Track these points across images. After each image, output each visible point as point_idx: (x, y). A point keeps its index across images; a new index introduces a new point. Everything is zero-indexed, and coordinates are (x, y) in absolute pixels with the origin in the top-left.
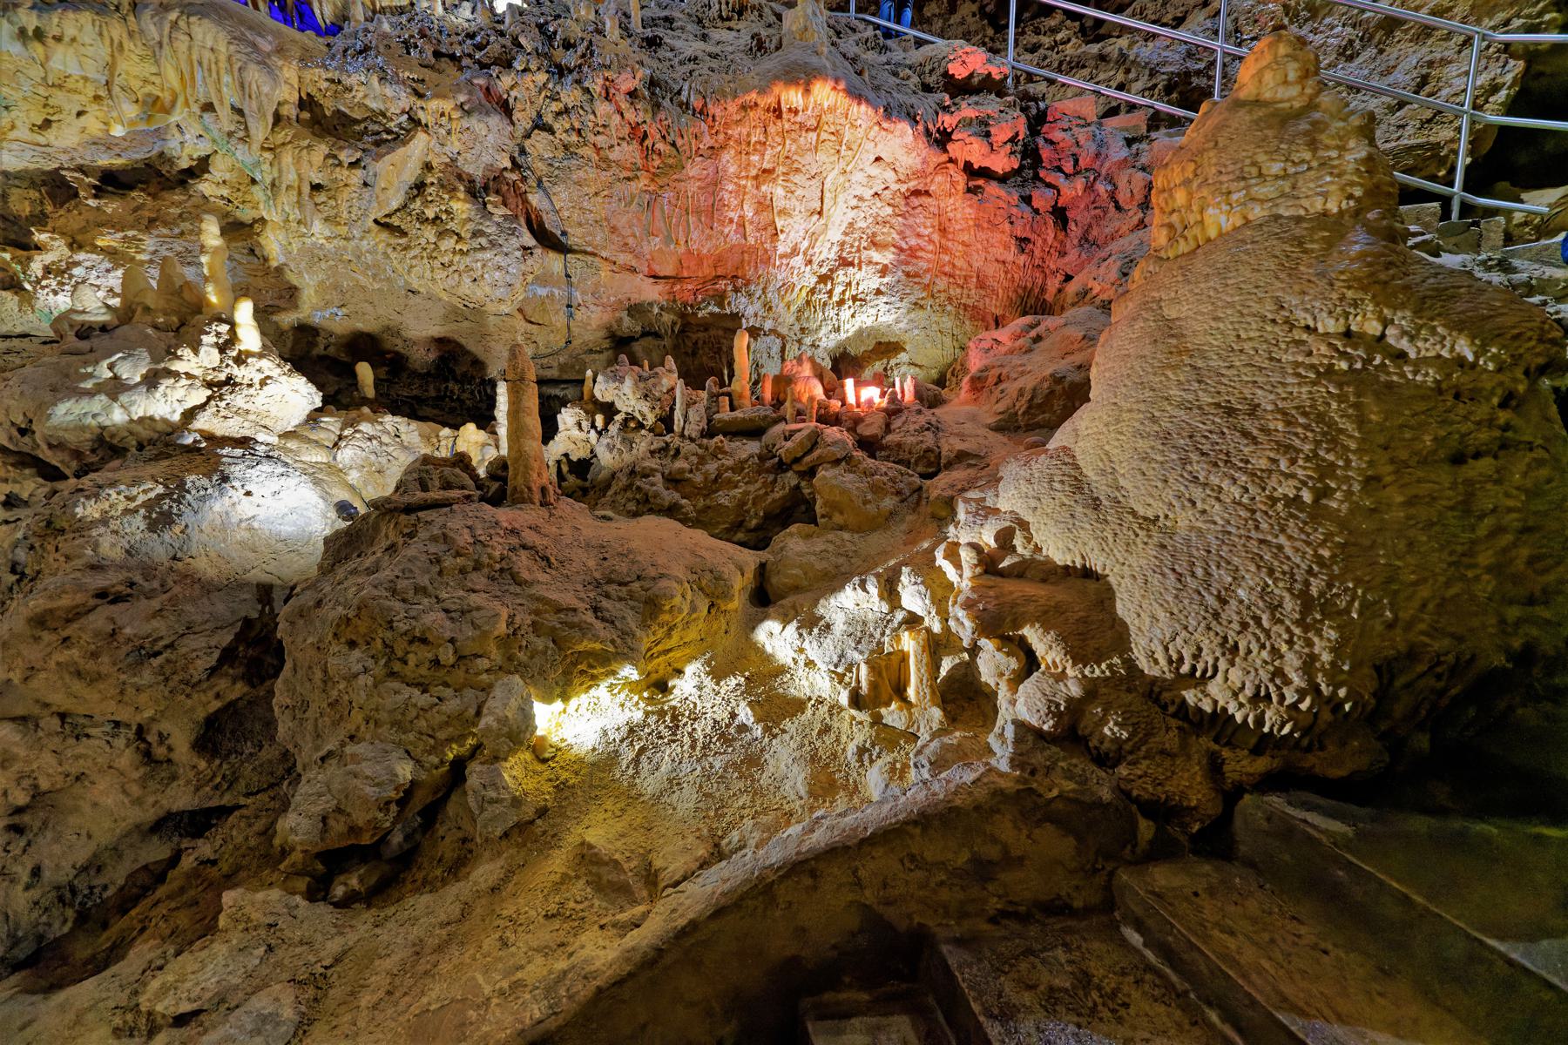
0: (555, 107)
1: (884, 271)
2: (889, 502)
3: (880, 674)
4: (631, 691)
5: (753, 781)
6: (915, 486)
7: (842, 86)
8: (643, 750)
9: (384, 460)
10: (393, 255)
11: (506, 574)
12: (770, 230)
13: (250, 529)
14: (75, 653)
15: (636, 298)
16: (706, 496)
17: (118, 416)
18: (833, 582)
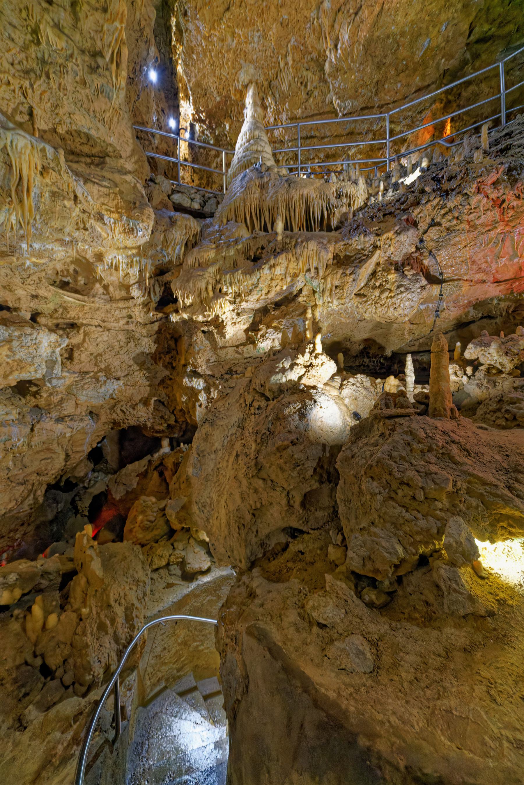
11: (446, 457)
17: (284, 380)
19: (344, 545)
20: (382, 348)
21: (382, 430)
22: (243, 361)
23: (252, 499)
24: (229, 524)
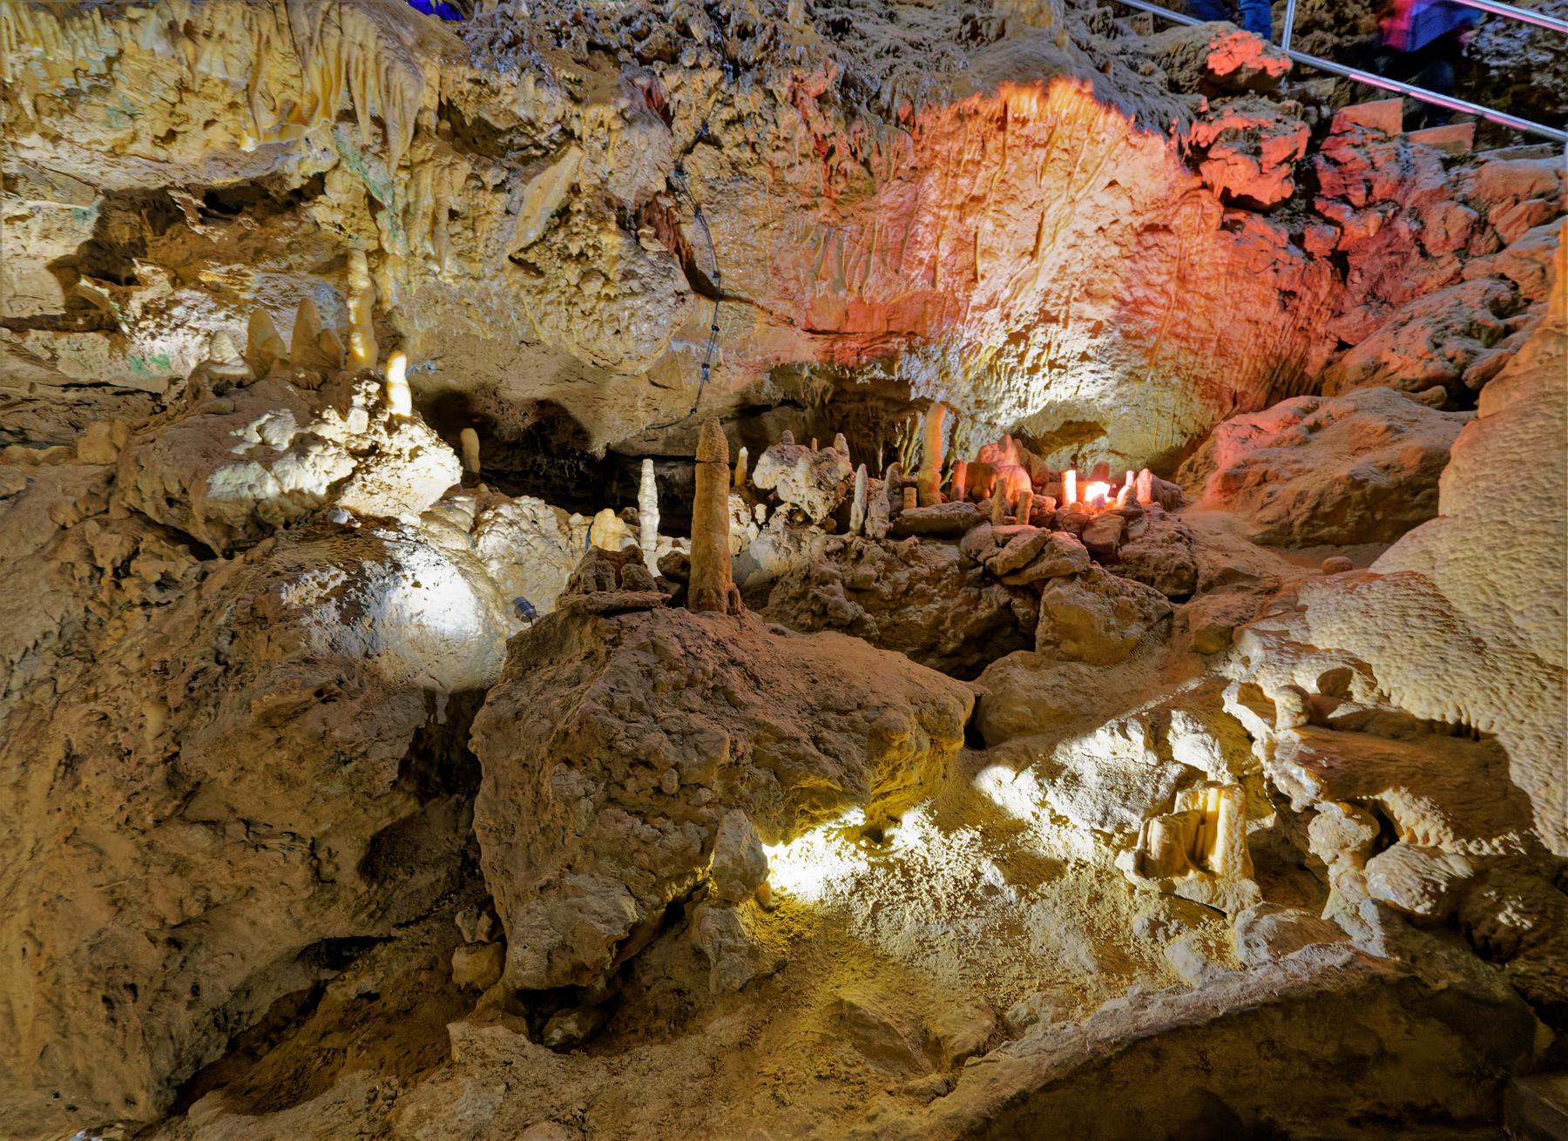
0: (727, 114)
1: (1096, 331)
2: (1135, 630)
3: (1176, 838)
4: (847, 838)
5: (1021, 949)
6: (1165, 611)
7: (1088, 89)
8: (877, 906)
9: (523, 550)
10: (527, 299)
11: (720, 694)
12: (968, 275)
13: (420, 625)
14: (284, 755)
15: (786, 358)
16: (892, 611)
17: (270, 489)
18: (1080, 723)
19: (498, 938)
20: (582, 435)
21: (589, 643)
22: (56, 393)
23: (166, 898)
24: (55, 1006)
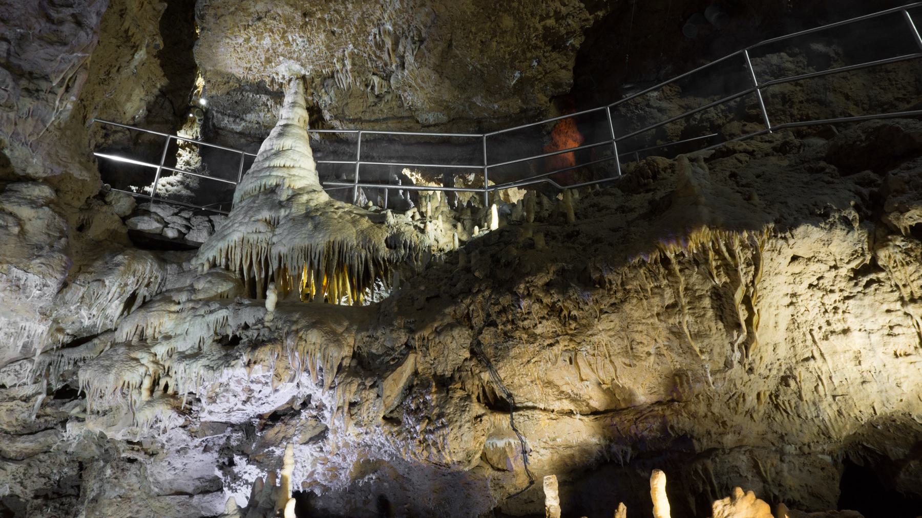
0: (497, 308)
